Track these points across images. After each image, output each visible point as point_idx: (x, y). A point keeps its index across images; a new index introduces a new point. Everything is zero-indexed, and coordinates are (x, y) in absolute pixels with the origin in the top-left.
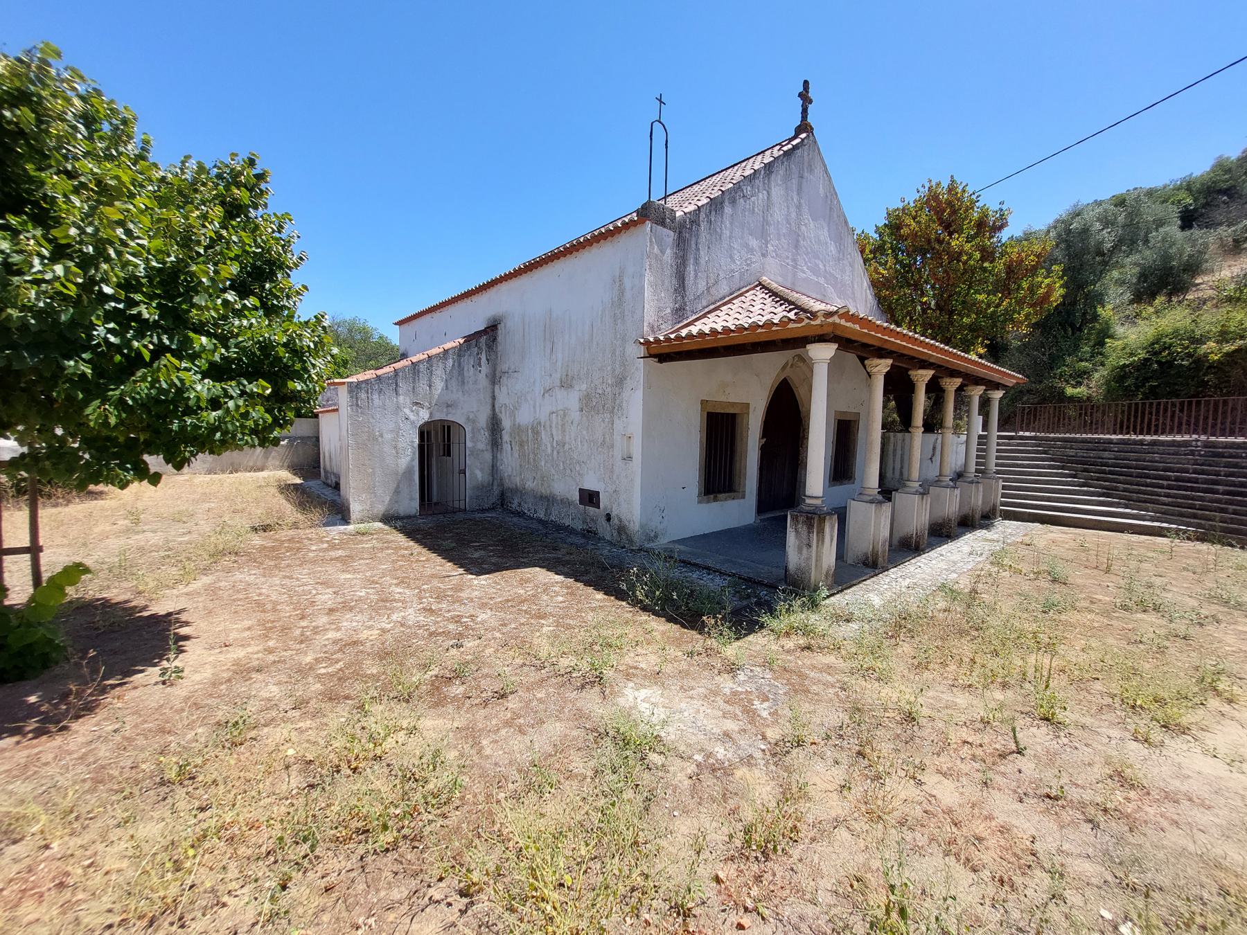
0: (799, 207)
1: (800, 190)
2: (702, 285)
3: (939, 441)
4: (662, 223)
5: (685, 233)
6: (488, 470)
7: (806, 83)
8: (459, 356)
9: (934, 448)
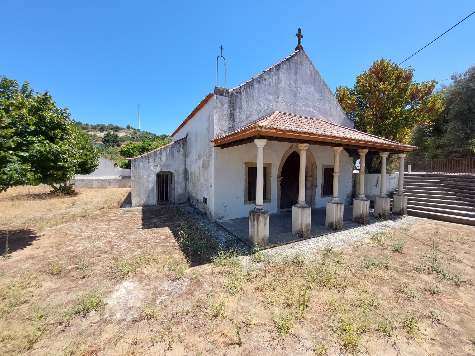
0: (296, 81)
1: (296, 74)
2: (243, 117)
3: (380, 177)
4: (222, 94)
5: (233, 98)
6: (183, 188)
7: (299, 30)
8: (172, 148)
9: (377, 181)
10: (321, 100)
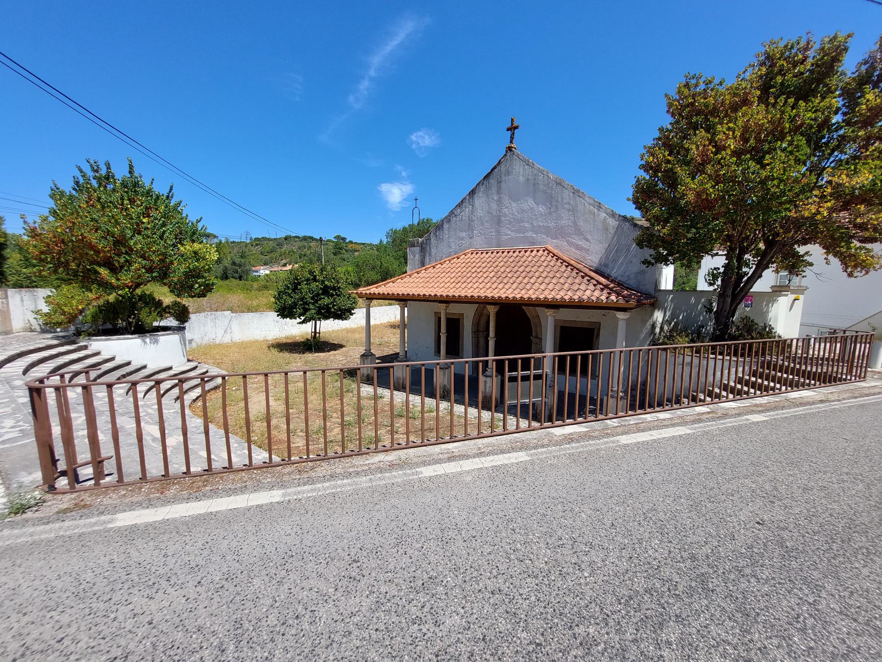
0: (499, 201)
1: (499, 192)
4: (414, 246)
10: (550, 213)
